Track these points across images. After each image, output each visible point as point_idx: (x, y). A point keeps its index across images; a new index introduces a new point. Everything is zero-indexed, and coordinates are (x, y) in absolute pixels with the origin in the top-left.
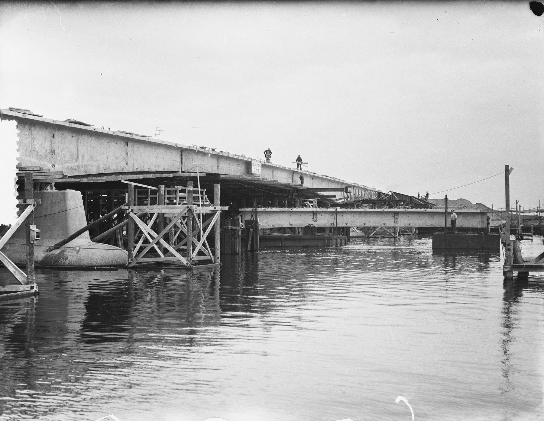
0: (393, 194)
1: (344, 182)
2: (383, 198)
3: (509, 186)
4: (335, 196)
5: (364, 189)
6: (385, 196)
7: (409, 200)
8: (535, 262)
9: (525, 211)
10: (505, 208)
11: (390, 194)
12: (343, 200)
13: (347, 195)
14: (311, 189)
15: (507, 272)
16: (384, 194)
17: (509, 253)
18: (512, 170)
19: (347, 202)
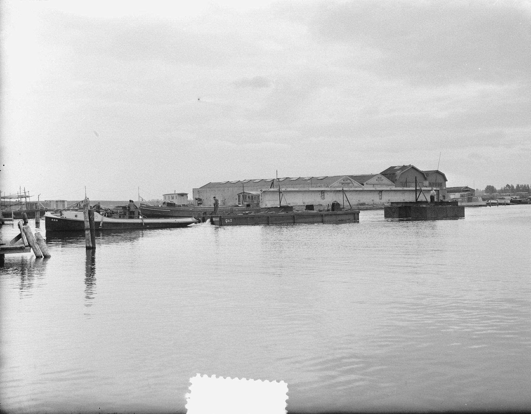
9: (6, 197)
14: (332, 177)
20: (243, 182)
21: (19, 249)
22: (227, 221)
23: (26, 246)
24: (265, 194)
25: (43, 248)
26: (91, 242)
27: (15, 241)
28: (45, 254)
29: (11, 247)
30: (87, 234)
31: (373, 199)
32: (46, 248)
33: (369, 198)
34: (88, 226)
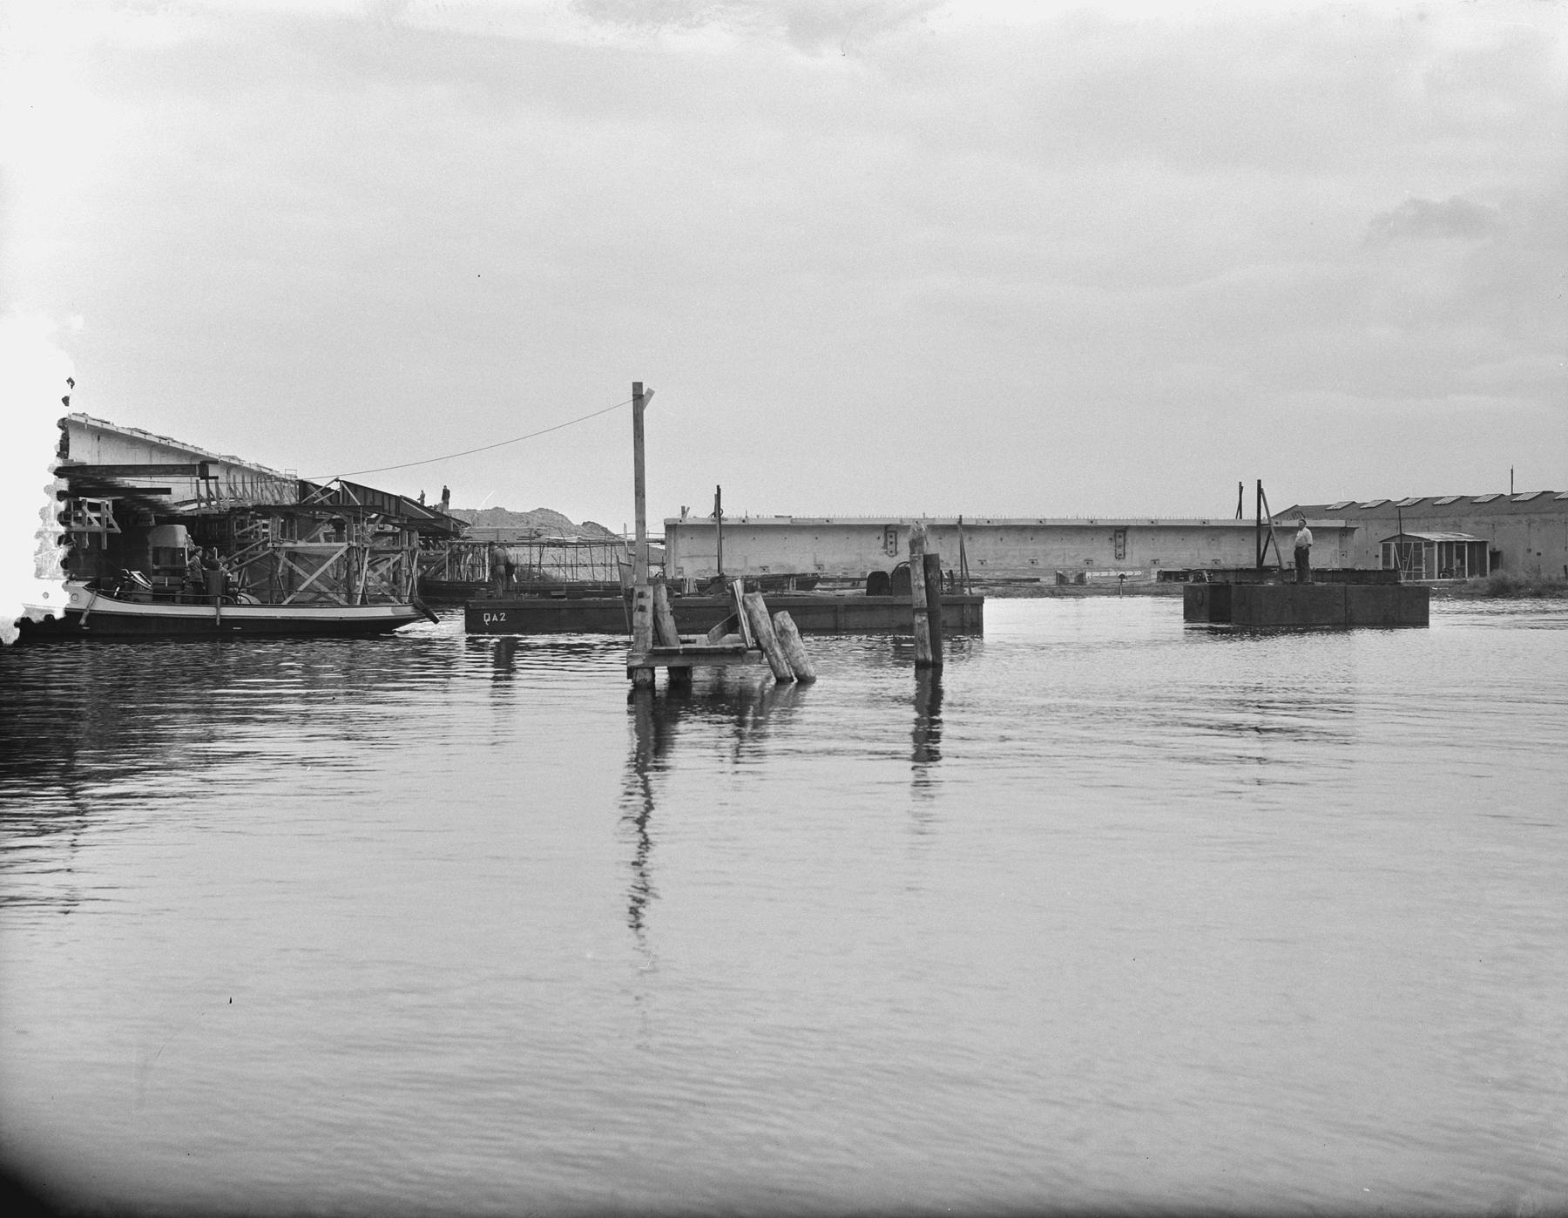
0: (343, 488)
1: (199, 452)
2: (314, 499)
3: (642, 440)
4: (168, 491)
5: (262, 476)
6: (321, 492)
7: (393, 508)
8: (708, 642)
10: (664, 532)
11: (336, 486)
12: (195, 506)
13: (209, 492)
15: (637, 668)
16: (318, 487)
17: (643, 617)
18: (651, 395)
19: (207, 510)
20: (1401, 504)
21: (730, 654)
22: (489, 620)
23: (752, 649)
24: (675, 534)
25: (796, 654)
26: (929, 649)
27: (721, 632)
28: (802, 673)
29: (712, 647)
30: (919, 624)
31: (1091, 556)
32: (803, 655)
33: (1072, 554)
34: (922, 602)
